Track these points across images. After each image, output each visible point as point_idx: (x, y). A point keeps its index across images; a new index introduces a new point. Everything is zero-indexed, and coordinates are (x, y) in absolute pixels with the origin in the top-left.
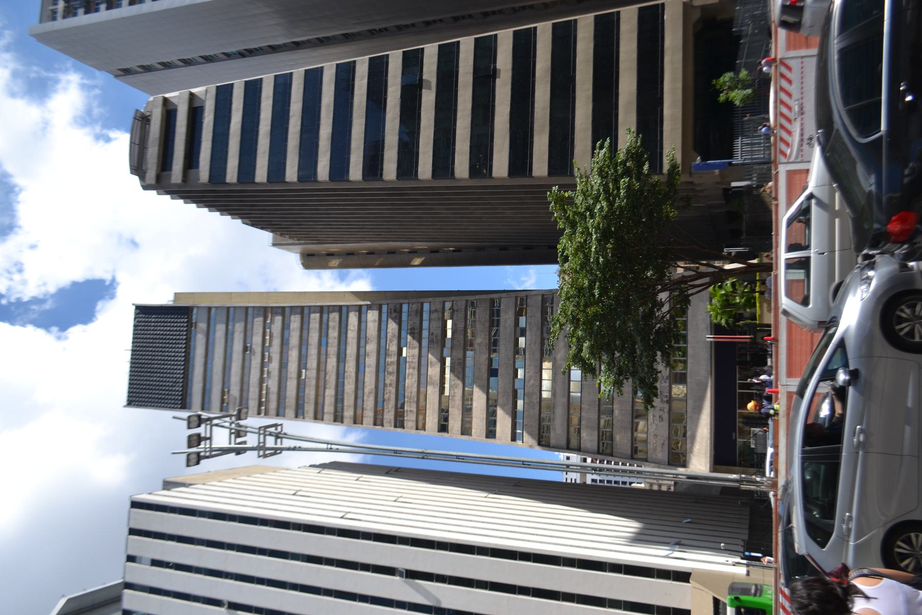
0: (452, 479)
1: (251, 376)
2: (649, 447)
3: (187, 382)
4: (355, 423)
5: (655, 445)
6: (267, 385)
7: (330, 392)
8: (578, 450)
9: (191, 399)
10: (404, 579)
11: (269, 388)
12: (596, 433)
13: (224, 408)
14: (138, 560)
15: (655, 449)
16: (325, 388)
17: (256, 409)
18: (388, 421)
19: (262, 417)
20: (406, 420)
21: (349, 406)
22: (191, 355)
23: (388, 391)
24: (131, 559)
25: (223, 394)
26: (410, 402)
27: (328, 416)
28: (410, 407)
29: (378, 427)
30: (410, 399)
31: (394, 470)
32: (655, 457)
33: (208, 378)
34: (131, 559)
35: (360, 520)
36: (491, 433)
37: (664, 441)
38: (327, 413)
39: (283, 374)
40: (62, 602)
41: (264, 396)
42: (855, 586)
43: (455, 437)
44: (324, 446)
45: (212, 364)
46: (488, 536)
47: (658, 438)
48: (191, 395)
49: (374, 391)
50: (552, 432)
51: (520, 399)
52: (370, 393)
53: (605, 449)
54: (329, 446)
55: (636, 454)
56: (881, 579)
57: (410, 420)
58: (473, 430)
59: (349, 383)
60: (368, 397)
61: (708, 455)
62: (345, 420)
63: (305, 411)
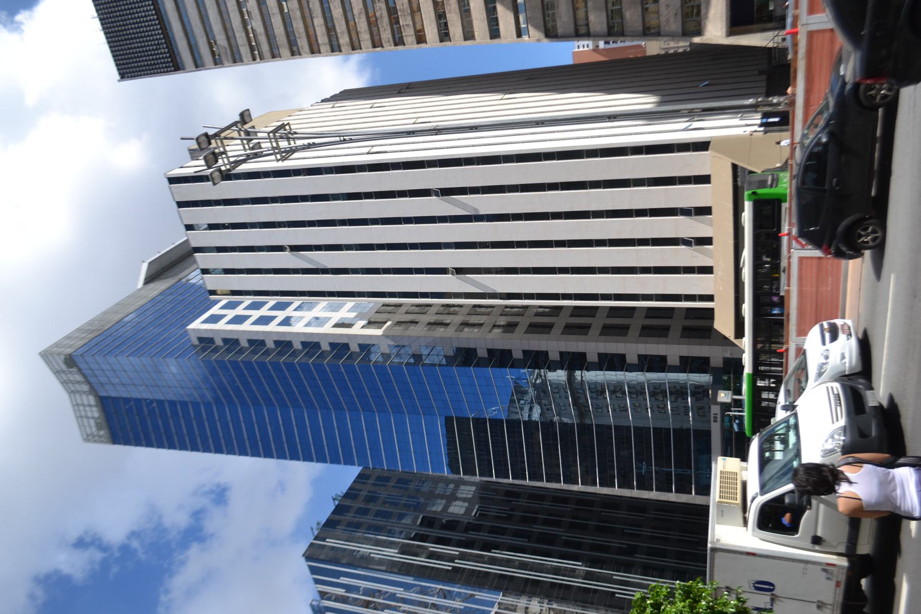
0: (465, 85)
1: (233, 21)
2: (661, 19)
3: (170, 42)
4: (353, 49)
5: (667, 17)
6: (252, 28)
7: (319, 21)
8: (588, 35)
9: (181, 59)
10: (441, 198)
11: (255, 30)
12: (604, 14)
13: (217, 61)
14: (196, 227)
15: (668, 21)
16: (312, 18)
17: (249, 55)
18: (387, 40)
19: (258, 63)
20: (405, 36)
21: (342, 33)
22: (163, 12)
23: (378, 8)
24: (189, 227)
25: (211, 47)
26: (404, 15)
27: (325, 48)
28: (405, 21)
29: (377, 49)
30: (403, 12)
31: (405, 87)
32: (668, 30)
33: (189, 31)
34: (189, 227)
35: (386, 152)
36: (495, 33)
37: (677, 11)
38: (323, 44)
39: (264, 11)
40: (145, 267)
41: (253, 39)
42: (842, 472)
43: (458, 45)
44: (337, 139)
45: (187, 16)
46: (511, 143)
47: (671, 8)
48: (179, 54)
49: (363, 11)
50: (558, 21)
51: (522, 12)
52: (360, 14)
53: (614, 30)
54: (342, 138)
55: (648, 32)
56: (861, 467)
57: (409, 35)
58: (476, 34)
59: (335, 7)
60: (360, 18)
61: (724, 18)
62: (343, 49)
63: (300, 47)
